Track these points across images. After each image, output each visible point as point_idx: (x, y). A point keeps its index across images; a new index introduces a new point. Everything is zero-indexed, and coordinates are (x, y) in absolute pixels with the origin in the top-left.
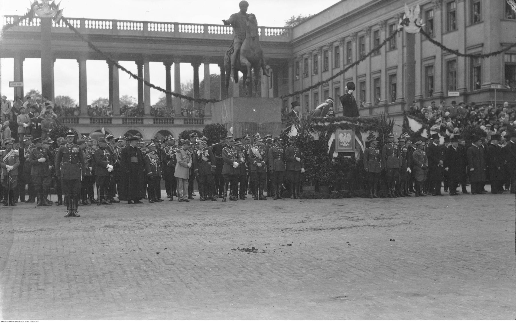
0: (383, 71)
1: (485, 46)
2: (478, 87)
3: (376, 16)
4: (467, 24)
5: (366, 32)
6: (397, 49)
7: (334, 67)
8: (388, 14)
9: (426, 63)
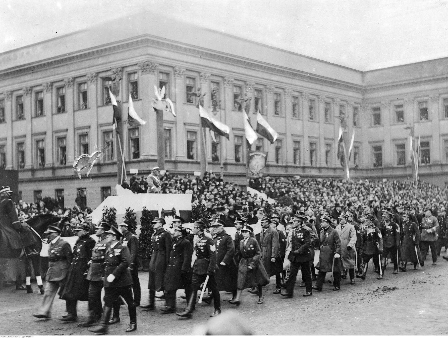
0: (49, 134)
1: (47, 133)
2: (137, 155)
3: (19, 81)
4: (14, 119)
5: (6, 96)
6: (6, 123)
7: (76, 109)
8: (35, 81)
9: (81, 131)
